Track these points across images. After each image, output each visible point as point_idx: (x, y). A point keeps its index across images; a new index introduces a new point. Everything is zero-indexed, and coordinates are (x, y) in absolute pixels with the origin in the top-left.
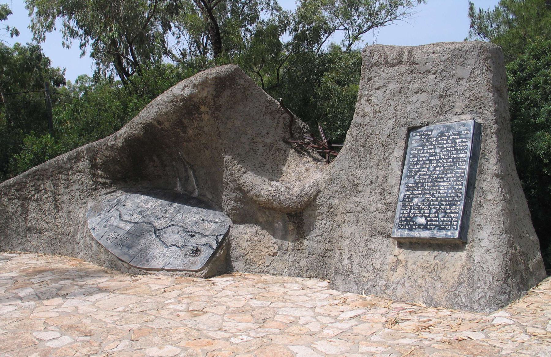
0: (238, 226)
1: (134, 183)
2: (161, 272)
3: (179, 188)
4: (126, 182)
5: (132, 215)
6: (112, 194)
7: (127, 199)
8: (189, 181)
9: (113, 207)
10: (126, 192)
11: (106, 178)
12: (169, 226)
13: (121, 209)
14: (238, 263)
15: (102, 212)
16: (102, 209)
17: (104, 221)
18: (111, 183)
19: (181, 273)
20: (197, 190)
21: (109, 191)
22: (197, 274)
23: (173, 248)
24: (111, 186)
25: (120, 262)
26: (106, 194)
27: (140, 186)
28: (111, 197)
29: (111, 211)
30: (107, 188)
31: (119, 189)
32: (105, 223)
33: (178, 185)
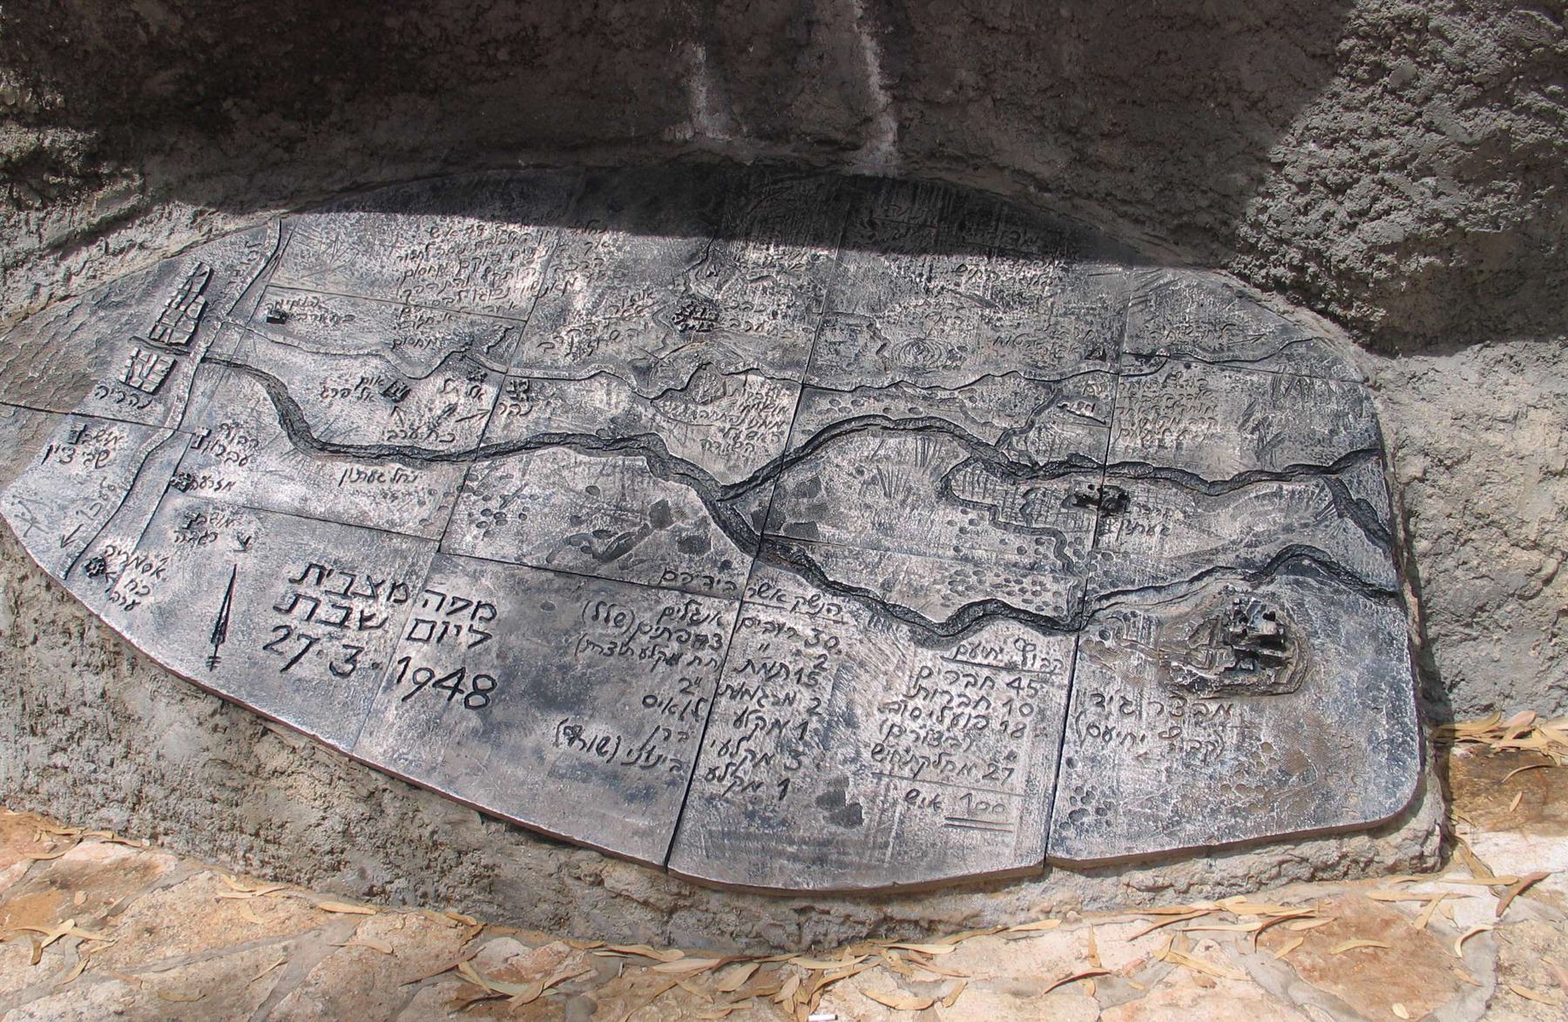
0: (1417, 364)
1: (292, 127)
2: (1030, 892)
3: (708, 123)
4: (213, 126)
5: (396, 394)
6: (114, 240)
7: (274, 260)
8: (806, 61)
9: (182, 350)
10: (237, 204)
11: (42, 120)
12: (817, 442)
13: (264, 350)
14: (1485, 648)
15: (95, 404)
16: (81, 383)
17: (159, 476)
18: (92, 158)
19: (1226, 866)
20: (889, 124)
21: (82, 217)
22: (1390, 848)
23: (1001, 636)
24: (93, 181)
25: (530, 854)
26: (63, 247)
27: (342, 143)
28: (117, 269)
29: (179, 387)
30: (65, 195)
31: (167, 195)
32: (179, 501)
33: (701, 96)
